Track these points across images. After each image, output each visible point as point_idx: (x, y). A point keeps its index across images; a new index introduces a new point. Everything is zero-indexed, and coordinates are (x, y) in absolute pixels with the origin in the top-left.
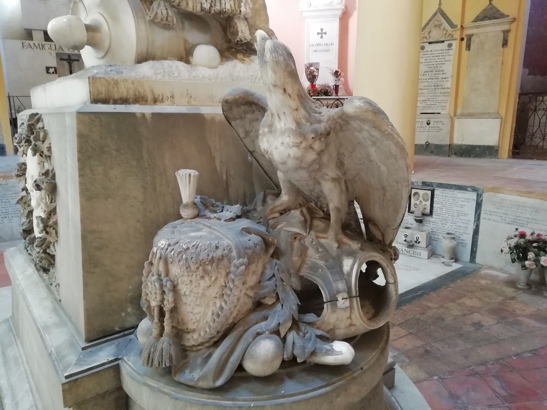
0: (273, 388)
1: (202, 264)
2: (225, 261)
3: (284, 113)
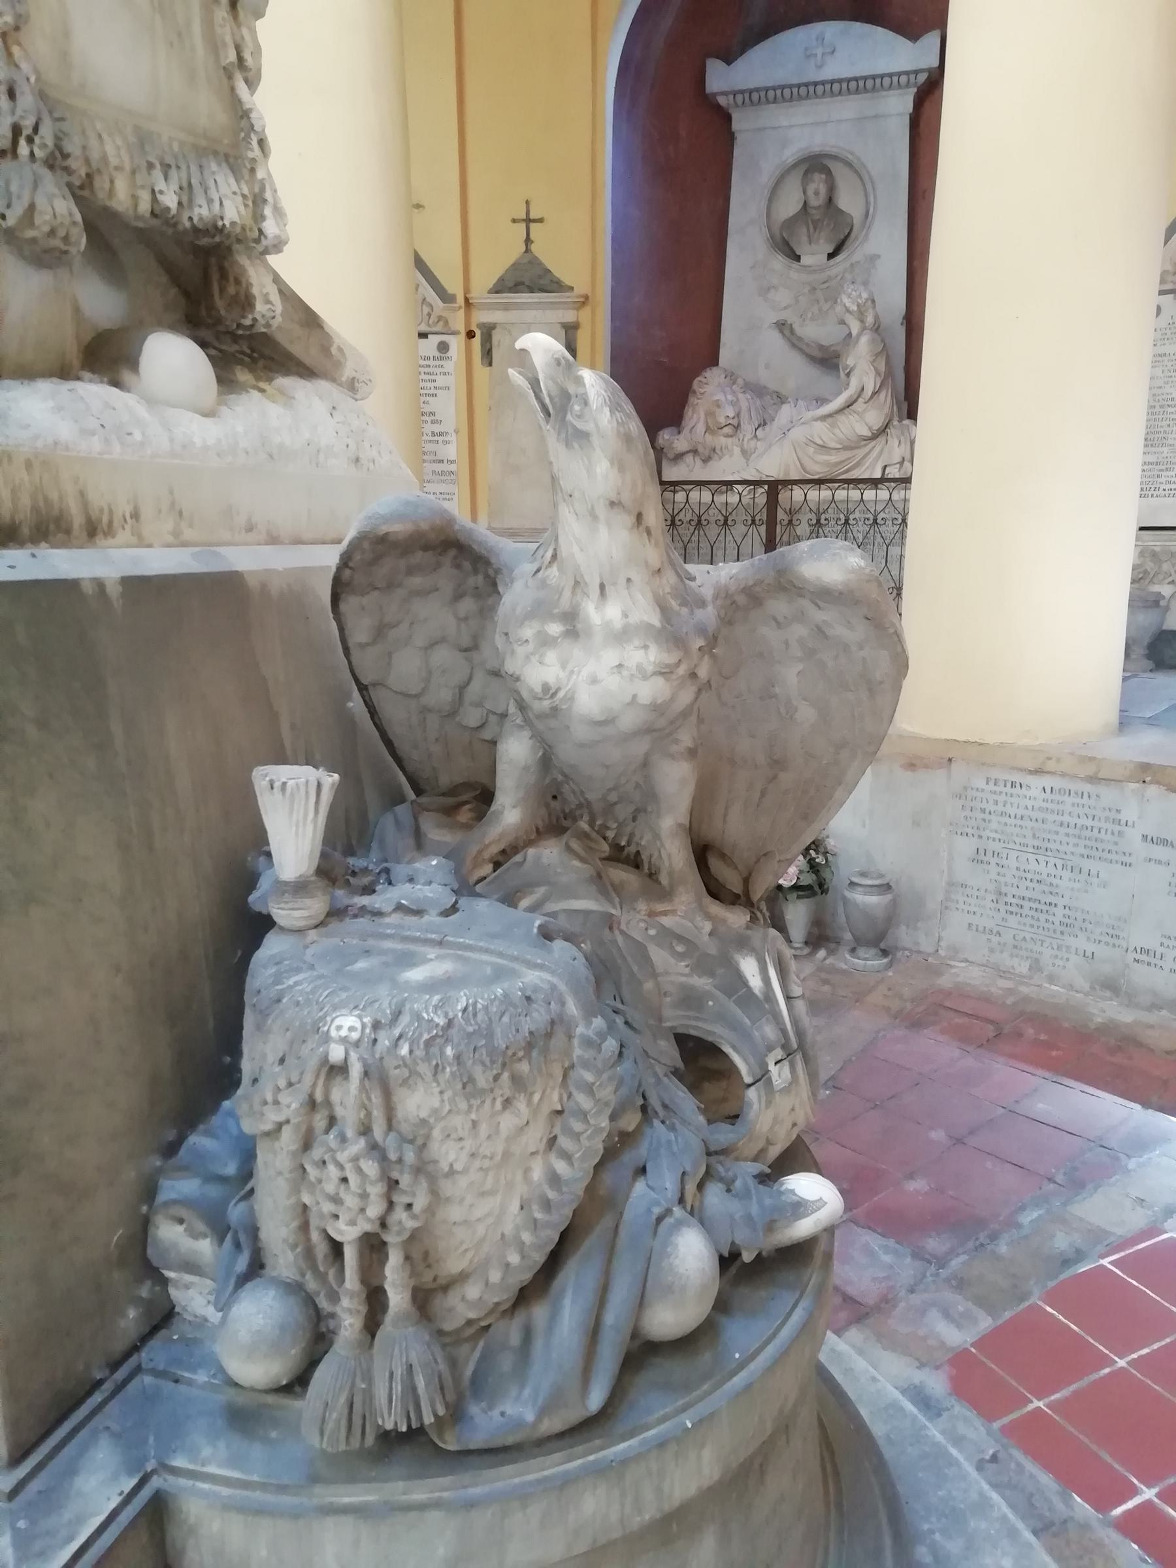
0: (707, 1356)
1: (505, 1060)
2: (558, 1041)
3: (629, 580)
